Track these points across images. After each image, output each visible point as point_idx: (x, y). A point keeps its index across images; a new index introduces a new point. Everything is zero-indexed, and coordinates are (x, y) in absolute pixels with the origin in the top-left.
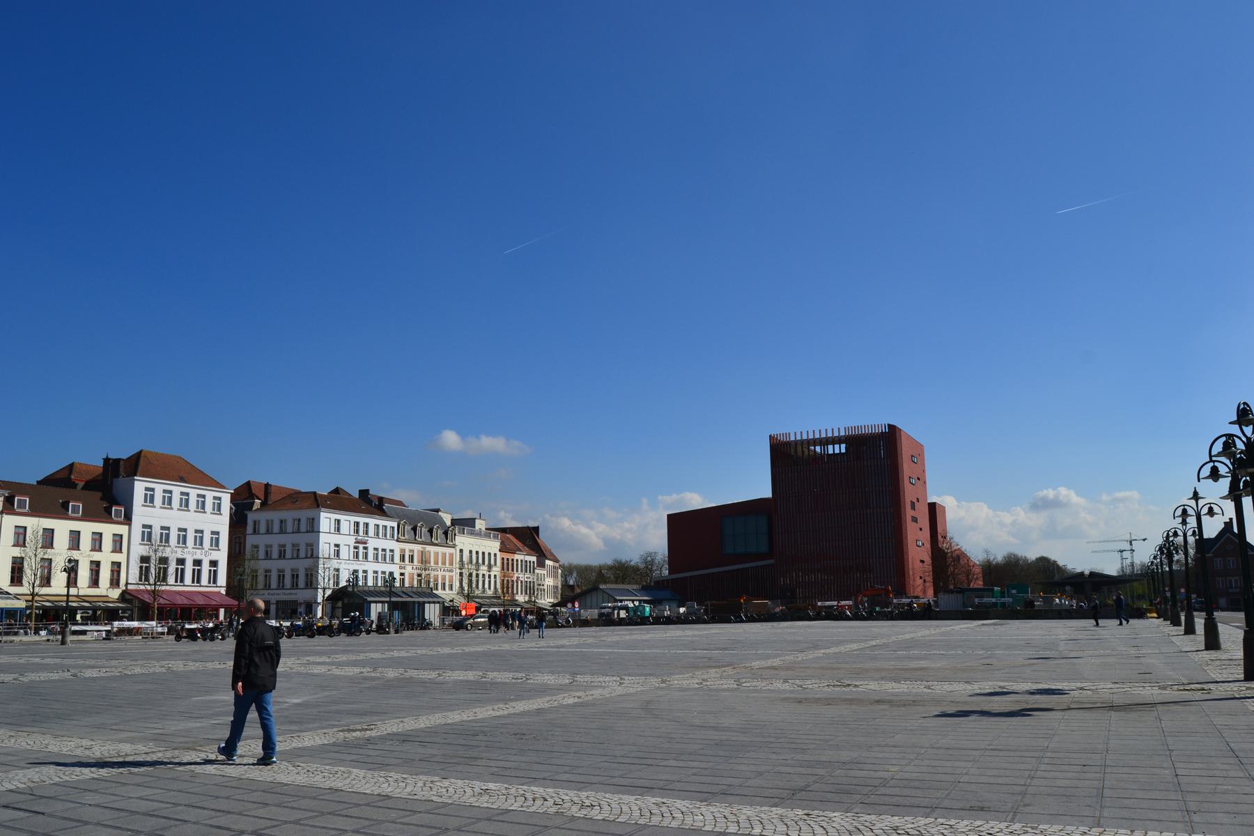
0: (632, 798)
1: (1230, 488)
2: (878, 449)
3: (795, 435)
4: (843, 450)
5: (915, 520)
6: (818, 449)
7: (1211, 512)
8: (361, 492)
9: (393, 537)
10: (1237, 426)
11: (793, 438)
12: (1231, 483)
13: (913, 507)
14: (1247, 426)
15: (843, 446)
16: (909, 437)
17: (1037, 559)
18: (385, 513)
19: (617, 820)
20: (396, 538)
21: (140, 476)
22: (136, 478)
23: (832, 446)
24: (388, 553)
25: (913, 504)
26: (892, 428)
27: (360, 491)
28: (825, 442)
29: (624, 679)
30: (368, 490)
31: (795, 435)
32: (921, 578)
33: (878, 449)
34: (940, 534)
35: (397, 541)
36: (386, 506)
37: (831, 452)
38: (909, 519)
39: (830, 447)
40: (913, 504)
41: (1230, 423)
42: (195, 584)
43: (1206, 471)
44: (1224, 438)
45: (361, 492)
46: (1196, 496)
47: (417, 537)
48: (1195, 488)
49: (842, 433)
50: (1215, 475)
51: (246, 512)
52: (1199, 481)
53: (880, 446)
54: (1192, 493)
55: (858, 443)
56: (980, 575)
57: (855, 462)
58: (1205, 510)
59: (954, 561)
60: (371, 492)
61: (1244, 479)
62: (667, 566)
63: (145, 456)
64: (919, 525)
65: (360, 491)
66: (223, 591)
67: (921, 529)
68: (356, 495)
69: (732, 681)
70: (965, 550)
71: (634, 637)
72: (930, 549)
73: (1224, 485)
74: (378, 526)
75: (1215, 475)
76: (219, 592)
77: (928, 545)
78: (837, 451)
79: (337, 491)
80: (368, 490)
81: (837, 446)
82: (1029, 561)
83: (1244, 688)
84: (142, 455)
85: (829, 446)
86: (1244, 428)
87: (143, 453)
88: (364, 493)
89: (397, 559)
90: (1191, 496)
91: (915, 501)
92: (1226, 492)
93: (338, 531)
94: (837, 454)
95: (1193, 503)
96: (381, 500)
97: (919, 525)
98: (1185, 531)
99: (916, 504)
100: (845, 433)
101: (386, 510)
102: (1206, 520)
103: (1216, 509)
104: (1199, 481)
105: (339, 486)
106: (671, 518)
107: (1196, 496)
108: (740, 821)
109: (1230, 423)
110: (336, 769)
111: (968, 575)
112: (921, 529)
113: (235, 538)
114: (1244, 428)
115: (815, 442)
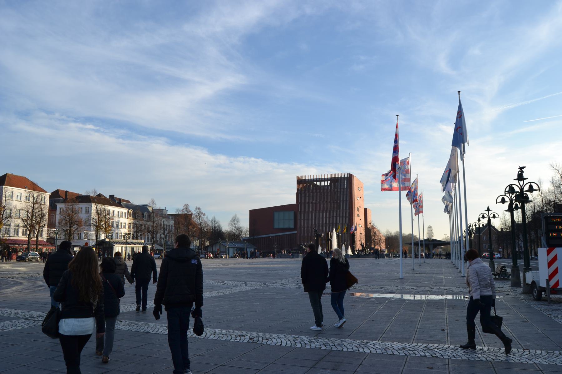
0: (282, 336)
1: (509, 207)
2: (344, 184)
3: (316, 176)
4: (329, 184)
5: (358, 216)
6: (318, 183)
7: (494, 217)
8: (110, 196)
9: (125, 217)
10: (517, 181)
11: (307, 178)
12: (509, 205)
13: (358, 210)
14: (521, 181)
15: (329, 182)
16: (358, 180)
17: (408, 234)
18: (122, 206)
19: (277, 344)
20: (127, 217)
21: (6, 186)
22: (4, 186)
23: (327, 182)
24: (123, 224)
25: (358, 209)
26: (351, 176)
27: (110, 195)
28: (321, 180)
29: (246, 283)
30: (114, 195)
31: (316, 176)
32: (360, 241)
33: (344, 184)
34: (369, 222)
35: (127, 218)
36: (122, 203)
37: (323, 185)
38: (356, 215)
39: (323, 182)
40: (358, 209)
41: (514, 180)
42: (24, 236)
43: (500, 199)
44: (508, 187)
45: (110, 196)
46: (488, 210)
47: (144, 218)
48: (488, 206)
49: (329, 177)
50: (503, 201)
51: (56, 204)
52: (496, 203)
53: (345, 183)
54: (487, 208)
55: (334, 181)
56: (385, 241)
57: (334, 190)
58: (492, 216)
59: (374, 234)
60: (115, 196)
61: (515, 203)
62: (249, 233)
63: (8, 176)
64: (360, 218)
65: (110, 195)
66: (45, 240)
67: (361, 220)
68: (108, 197)
69: (295, 285)
70: (379, 229)
71: (282, 265)
72: (364, 228)
73: (506, 206)
74: (119, 212)
75: (503, 201)
76: (43, 241)
77: (364, 227)
78: (326, 184)
79: (445, 211)
80: (114, 195)
81: (326, 182)
82: (405, 235)
83: (512, 290)
84: (7, 176)
85: (323, 182)
86: (520, 181)
87: (7, 175)
88: (112, 196)
89: (127, 227)
90: (486, 209)
91: (359, 207)
92: (507, 208)
93: (109, 215)
94: (326, 186)
95: (487, 212)
96: (120, 200)
97: (360, 218)
98: (521, 187)
99: (359, 209)
100: (330, 176)
101: (122, 205)
102: (492, 220)
103: (496, 215)
104: (496, 203)
105: (100, 193)
106: (250, 210)
107: (488, 210)
108: (336, 345)
109: (514, 180)
110: (140, 323)
111: (380, 240)
112: (361, 220)
113: (51, 216)
114: (520, 181)
115: (317, 180)
